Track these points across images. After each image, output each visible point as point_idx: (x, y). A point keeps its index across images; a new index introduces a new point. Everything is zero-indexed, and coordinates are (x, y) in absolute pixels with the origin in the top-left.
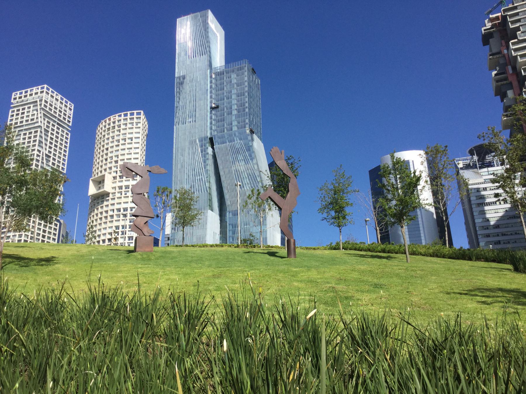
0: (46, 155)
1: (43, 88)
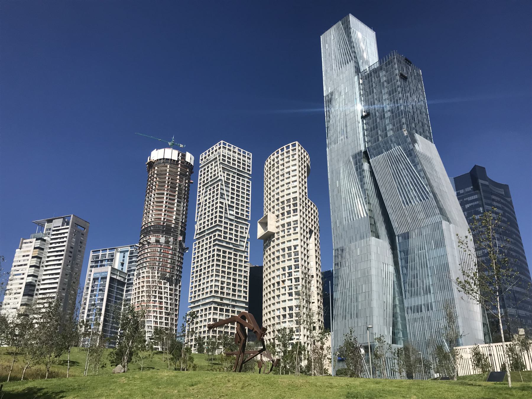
0: (229, 206)
1: (220, 144)
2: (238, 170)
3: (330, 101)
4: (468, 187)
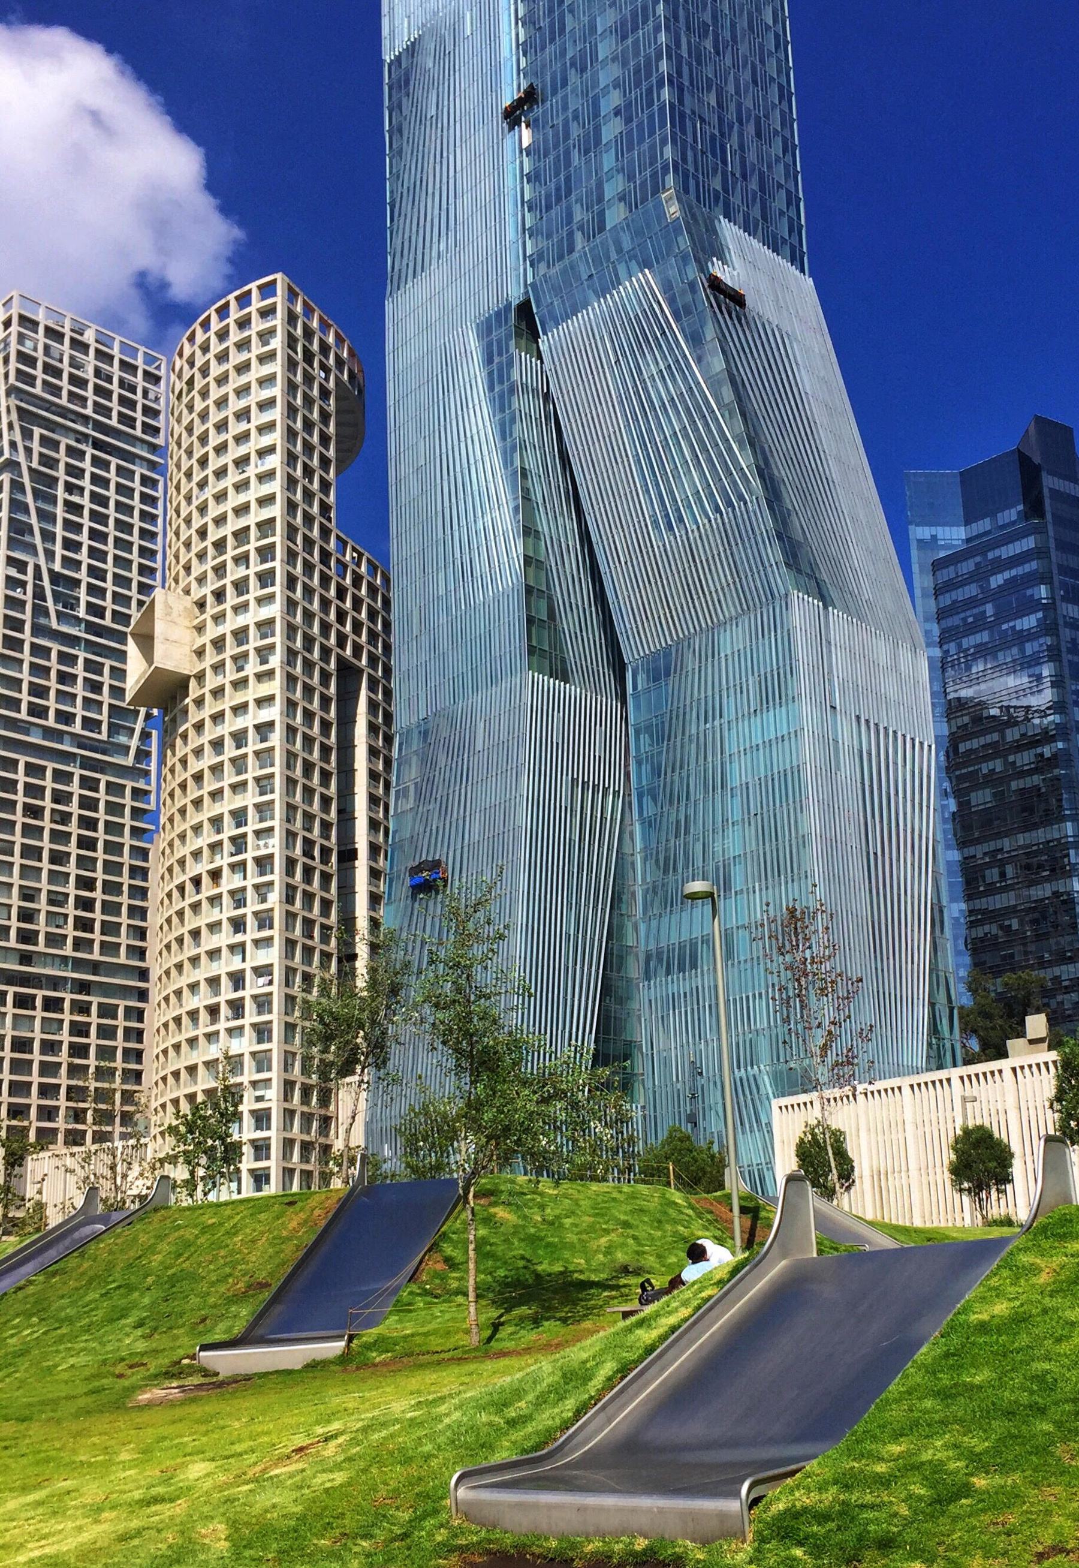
0: (56, 578)
2: (99, 426)
3: (403, 83)
4: (1009, 507)
